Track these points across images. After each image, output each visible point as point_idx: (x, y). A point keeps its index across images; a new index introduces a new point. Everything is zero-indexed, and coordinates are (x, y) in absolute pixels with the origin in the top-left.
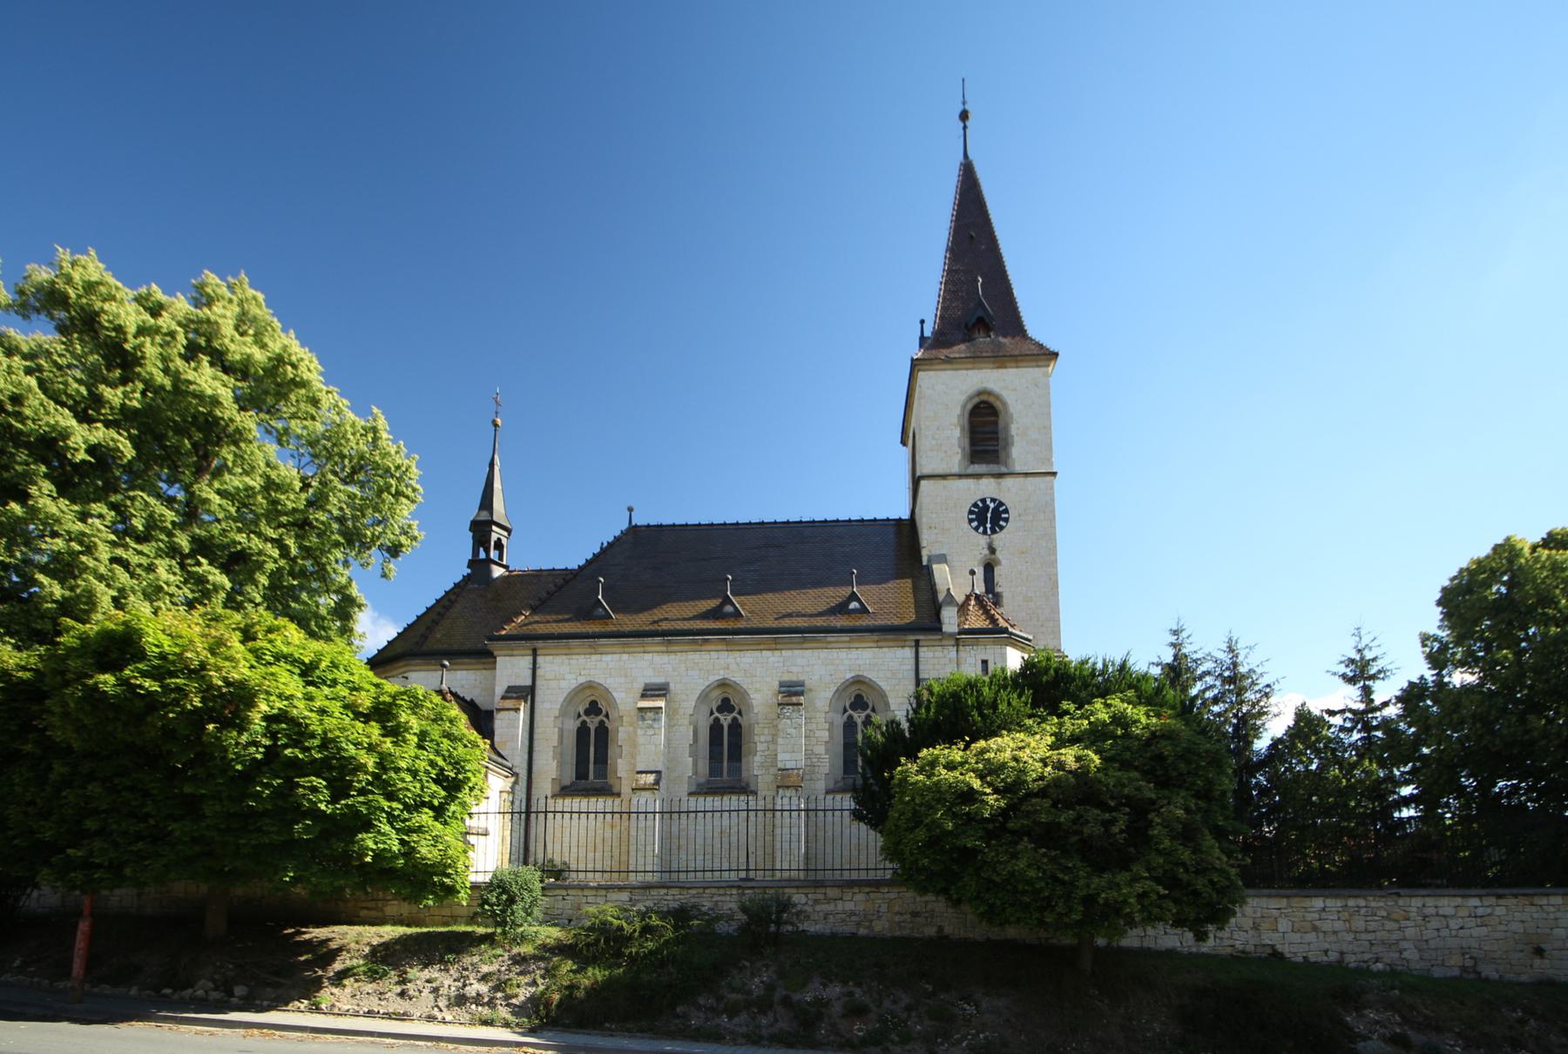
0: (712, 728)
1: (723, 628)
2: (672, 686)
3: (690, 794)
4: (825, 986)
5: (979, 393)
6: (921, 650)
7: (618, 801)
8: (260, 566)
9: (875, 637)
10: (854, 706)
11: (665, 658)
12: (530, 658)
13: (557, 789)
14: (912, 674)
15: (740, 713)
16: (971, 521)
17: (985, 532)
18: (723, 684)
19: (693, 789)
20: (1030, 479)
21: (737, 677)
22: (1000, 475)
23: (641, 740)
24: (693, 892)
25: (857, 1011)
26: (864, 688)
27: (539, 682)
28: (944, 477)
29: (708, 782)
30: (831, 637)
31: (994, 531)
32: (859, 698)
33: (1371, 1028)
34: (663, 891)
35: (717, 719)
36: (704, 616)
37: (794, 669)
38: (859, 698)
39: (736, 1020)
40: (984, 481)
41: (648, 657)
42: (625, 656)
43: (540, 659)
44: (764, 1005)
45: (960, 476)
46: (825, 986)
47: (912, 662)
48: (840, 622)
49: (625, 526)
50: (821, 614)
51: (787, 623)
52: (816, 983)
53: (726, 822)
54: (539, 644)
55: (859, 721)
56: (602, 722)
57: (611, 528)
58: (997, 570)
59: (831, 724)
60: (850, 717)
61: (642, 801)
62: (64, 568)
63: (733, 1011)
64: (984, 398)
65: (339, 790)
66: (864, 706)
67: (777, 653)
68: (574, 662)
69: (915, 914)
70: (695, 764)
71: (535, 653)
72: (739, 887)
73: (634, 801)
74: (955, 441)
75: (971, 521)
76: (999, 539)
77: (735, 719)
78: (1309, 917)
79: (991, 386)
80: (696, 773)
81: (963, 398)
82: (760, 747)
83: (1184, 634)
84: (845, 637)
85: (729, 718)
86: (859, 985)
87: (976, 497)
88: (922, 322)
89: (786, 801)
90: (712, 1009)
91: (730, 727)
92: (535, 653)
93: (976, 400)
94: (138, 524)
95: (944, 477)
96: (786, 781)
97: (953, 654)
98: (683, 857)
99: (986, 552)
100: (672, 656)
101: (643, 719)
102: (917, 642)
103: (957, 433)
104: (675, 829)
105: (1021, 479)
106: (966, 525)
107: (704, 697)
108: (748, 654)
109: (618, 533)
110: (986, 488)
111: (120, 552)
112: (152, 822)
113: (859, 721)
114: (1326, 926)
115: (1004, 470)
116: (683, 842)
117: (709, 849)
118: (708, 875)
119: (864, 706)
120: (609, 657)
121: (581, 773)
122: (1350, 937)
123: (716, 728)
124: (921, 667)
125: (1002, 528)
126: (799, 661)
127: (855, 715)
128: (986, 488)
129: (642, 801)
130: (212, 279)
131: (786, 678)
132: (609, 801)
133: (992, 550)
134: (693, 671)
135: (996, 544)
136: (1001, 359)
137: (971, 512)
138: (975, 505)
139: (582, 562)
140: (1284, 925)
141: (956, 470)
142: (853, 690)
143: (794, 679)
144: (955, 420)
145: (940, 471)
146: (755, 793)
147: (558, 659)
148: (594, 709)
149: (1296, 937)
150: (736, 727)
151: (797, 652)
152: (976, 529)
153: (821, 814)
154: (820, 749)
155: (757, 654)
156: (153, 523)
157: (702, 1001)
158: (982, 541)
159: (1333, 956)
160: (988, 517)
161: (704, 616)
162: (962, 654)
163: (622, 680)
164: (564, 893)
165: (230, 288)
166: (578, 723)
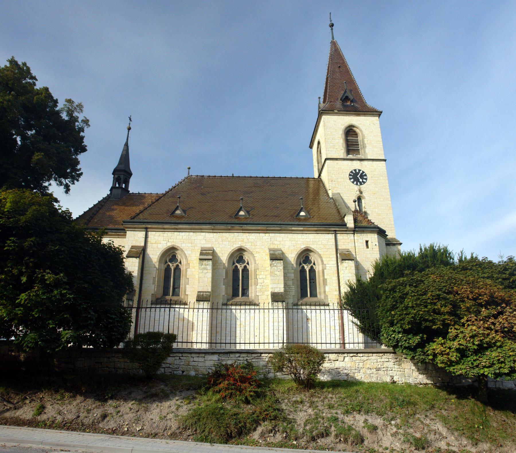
1: (232, 223)
11: (211, 235)
13: (154, 299)
14: (334, 247)
16: (350, 179)
27: (149, 244)
34: (237, 355)
37: (276, 242)
47: (334, 240)
49: (186, 176)
57: (181, 176)
58: (363, 201)
69: (378, 369)
70: (226, 289)
74: (341, 145)
75: (350, 179)
76: (363, 187)
80: (227, 294)
87: (352, 169)
88: (320, 98)
93: (348, 129)
99: (358, 192)
100: (215, 234)
106: (348, 180)
107: (232, 256)
108: (253, 234)
110: (356, 165)
113: (172, 268)
116: (219, 330)
118: (333, 345)
120: (183, 233)
121: (166, 292)
126: (278, 239)
127: (239, 266)
128: (356, 165)
133: (361, 192)
134: (224, 243)
135: (362, 190)
137: (350, 175)
138: (352, 172)
141: (342, 157)
143: (276, 247)
144: (340, 136)
145: (335, 157)
154: (290, 283)
155: (258, 234)
158: (356, 188)
163: (190, 245)
164: (181, 355)
166: (166, 266)
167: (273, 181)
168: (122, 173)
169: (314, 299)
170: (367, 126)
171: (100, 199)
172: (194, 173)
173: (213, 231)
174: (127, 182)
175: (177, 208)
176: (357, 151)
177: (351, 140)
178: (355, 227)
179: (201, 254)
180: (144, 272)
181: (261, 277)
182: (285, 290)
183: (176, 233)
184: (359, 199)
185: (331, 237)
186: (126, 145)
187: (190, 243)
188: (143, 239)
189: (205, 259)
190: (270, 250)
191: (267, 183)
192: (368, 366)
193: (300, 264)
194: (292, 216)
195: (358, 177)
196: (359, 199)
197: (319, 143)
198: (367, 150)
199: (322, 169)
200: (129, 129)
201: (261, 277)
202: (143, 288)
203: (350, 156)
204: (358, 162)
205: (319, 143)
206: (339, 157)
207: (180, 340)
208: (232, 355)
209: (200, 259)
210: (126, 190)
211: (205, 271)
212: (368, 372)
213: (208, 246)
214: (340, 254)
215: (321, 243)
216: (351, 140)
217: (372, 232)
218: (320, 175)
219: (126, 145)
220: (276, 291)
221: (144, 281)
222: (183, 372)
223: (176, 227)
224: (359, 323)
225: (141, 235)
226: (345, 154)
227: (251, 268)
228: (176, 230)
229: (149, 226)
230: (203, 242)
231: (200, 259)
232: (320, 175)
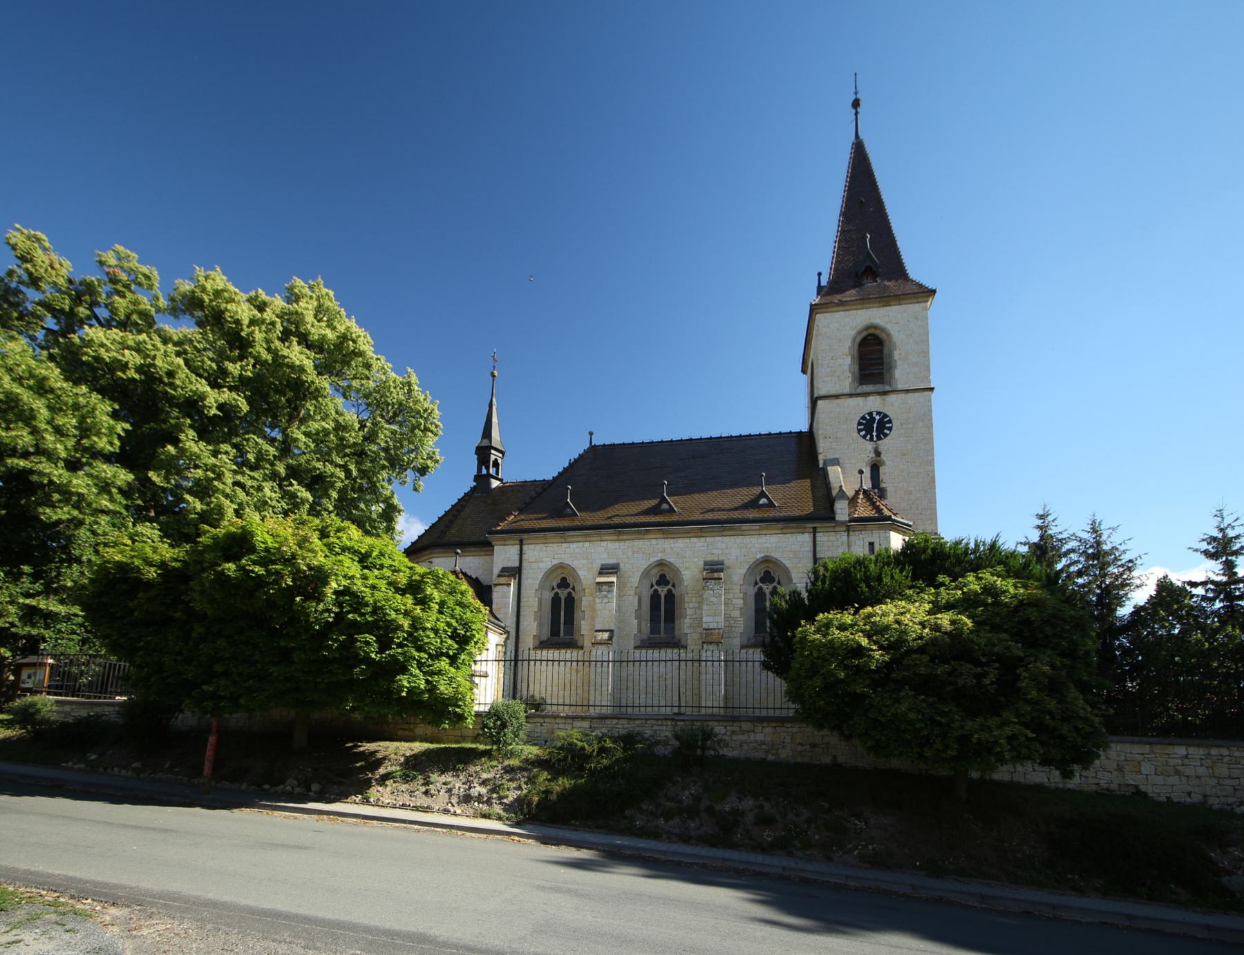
1: (661, 521)
2: (622, 566)
3: (636, 648)
4: (740, 799)
5: (867, 328)
6: (818, 535)
7: (581, 652)
8: (332, 485)
9: (780, 525)
11: (617, 544)
13: (537, 643)
14: (811, 555)
17: (872, 439)
18: (661, 564)
19: (745, 642)
20: (910, 395)
22: (885, 393)
25: (766, 821)
28: (837, 397)
30: (745, 527)
31: (879, 438)
32: (767, 573)
35: (656, 591)
36: (647, 512)
37: (716, 551)
38: (767, 573)
39: (671, 823)
40: (871, 398)
42: (587, 544)
43: (525, 547)
45: (851, 395)
46: (740, 799)
47: (811, 544)
48: (752, 514)
49: (587, 446)
50: (736, 509)
51: (710, 516)
54: (525, 536)
55: (767, 592)
56: (570, 593)
57: (577, 448)
58: (882, 470)
59: (745, 594)
61: (599, 653)
62: (203, 490)
65: (384, 645)
69: (814, 745)
70: (639, 625)
71: (521, 543)
72: (673, 720)
73: (593, 653)
74: (846, 368)
75: (859, 431)
76: (884, 444)
78: (1172, 762)
79: (878, 321)
80: (640, 631)
81: (854, 333)
83: (1050, 518)
84: (756, 526)
85: (665, 590)
88: (820, 274)
91: (666, 596)
92: (521, 543)
93: (864, 334)
94: (251, 457)
95: (837, 397)
96: (710, 638)
97: (845, 538)
99: (872, 455)
100: (622, 543)
102: (815, 529)
103: (848, 361)
105: (903, 396)
106: (856, 434)
107: (646, 573)
108: (680, 540)
109: (581, 452)
110: (873, 404)
111: (239, 477)
112: (259, 666)
113: (767, 592)
114: (1189, 771)
115: (888, 388)
116: (630, 684)
122: (1213, 782)
123: (655, 597)
124: (818, 549)
125: (886, 435)
128: (873, 404)
130: (299, 282)
131: (709, 558)
132: (575, 652)
133: (878, 453)
134: (637, 554)
135: (881, 449)
137: (859, 424)
138: (863, 418)
139: (556, 474)
140: (1147, 768)
141: (847, 391)
144: (846, 351)
145: (833, 392)
148: (564, 583)
149: (1159, 780)
150: (670, 597)
154: (736, 614)
155: (687, 540)
156: (260, 456)
157: (644, 807)
158: (869, 446)
159: (1196, 798)
160: (875, 427)
161: (647, 512)
162: (852, 538)
163: (584, 562)
165: (311, 288)
166: (552, 594)
171: (461, 495)
172: (598, 441)
180: (522, 604)
183: (564, 545)
185: (807, 538)
188: (517, 557)
192: (798, 740)
198: (898, 373)
202: (521, 628)
203: (866, 388)
204: (878, 397)
206: (840, 392)
207: (757, 664)
211: (606, 600)
212: (799, 748)
221: (522, 618)
225: (513, 550)
227: (676, 592)
230: (605, 556)
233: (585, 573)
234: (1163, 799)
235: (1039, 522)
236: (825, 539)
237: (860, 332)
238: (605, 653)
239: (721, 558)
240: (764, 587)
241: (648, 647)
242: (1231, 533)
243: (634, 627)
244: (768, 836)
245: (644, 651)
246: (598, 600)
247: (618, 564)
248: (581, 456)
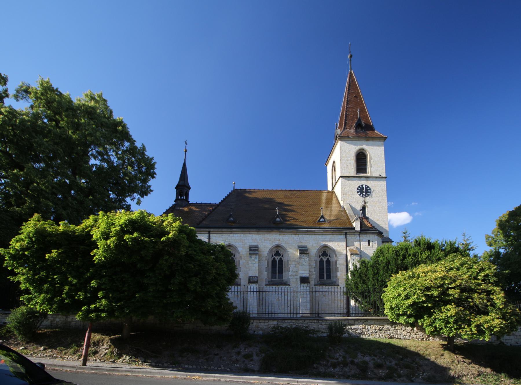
0: (320, 261)
2: (259, 246)
3: (266, 285)
4: (364, 357)
6: (347, 236)
7: (239, 287)
10: (276, 255)
11: (257, 236)
12: (208, 235)
15: (282, 256)
16: (358, 192)
17: (363, 196)
18: (278, 246)
19: (267, 283)
21: (283, 244)
23: (250, 265)
24: (300, 321)
25: (379, 366)
26: (327, 249)
29: (272, 281)
31: (366, 196)
32: (325, 252)
33: (255, 365)
34: (289, 321)
35: (274, 258)
37: (303, 241)
38: (325, 252)
39: (336, 370)
41: (251, 235)
42: (242, 235)
43: (211, 235)
44: (345, 364)
46: (364, 357)
49: (232, 189)
52: (360, 355)
53: (280, 296)
55: (325, 261)
56: (281, 258)
59: (316, 261)
60: (322, 259)
61: (252, 287)
63: (334, 366)
64: (362, 151)
66: (327, 255)
67: (297, 235)
68: (223, 236)
70: (268, 274)
71: (209, 234)
72: (318, 320)
73: (249, 287)
75: (358, 192)
76: (367, 199)
77: (281, 258)
80: (268, 277)
82: (291, 269)
83: (408, 233)
85: (279, 258)
86: (376, 356)
89: (302, 288)
90: (326, 365)
91: (279, 261)
92: (209, 234)
96: (252, 280)
97: (358, 238)
98: (264, 308)
99: (363, 203)
100: (259, 236)
101: (251, 258)
102: (346, 233)
104: (261, 297)
106: (356, 193)
107: (271, 250)
108: (287, 235)
109: (230, 192)
110: (364, 183)
112: (126, 293)
113: (325, 261)
116: (264, 302)
117: (273, 305)
119: (327, 255)
120: (237, 235)
123: (274, 261)
128: (364, 183)
129: (252, 287)
131: (300, 244)
132: (236, 287)
133: (365, 203)
134: (266, 241)
135: (366, 201)
136: (368, 139)
137: (358, 189)
138: (359, 187)
139: (220, 201)
142: (323, 250)
143: (303, 245)
144: (352, 158)
146: (289, 285)
147: (218, 235)
148: (277, 254)
150: (281, 261)
151: (304, 235)
152: (360, 195)
153: (336, 293)
154: (313, 270)
155: (290, 235)
157: (322, 363)
158: (362, 199)
162: (361, 238)
163: (241, 243)
167: (298, 194)
168: (183, 188)
169: (329, 281)
170: (376, 154)
172: (236, 188)
173: (258, 233)
174: (187, 195)
175: (231, 216)
176: (365, 171)
177: (361, 161)
178: (361, 230)
179: (250, 250)
181: (292, 266)
182: (309, 275)
183: (231, 235)
184: (364, 208)
186: (184, 165)
187: (239, 241)
189: (254, 254)
190: (299, 247)
191: (294, 195)
193: (320, 257)
194: (314, 221)
195: (364, 191)
196: (364, 208)
197: (334, 162)
199: (336, 183)
200: (186, 151)
201: (292, 266)
205: (334, 162)
206: (350, 175)
208: (286, 321)
209: (250, 254)
210: (187, 200)
211: (254, 262)
213: (255, 244)
214: (349, 250)
215: (338, 245)
216: (361, 161)
217: (373, 234)
218: (333, 188)
219: (184, 165)
220: (304, 275)
222: (254, 332)
223: (231, 230)
224: (247, 195)
226: (355, 172)
227: (284, 259)
228: (232, 232)
229: (212, 230)
231: (250, 254)
232: (333, 188)
233: (241, 249)
234: (509, 345)
235: (404, 235)
236: (350, 238)
237: (357, 151)
238: (255, 287)
239: (305, 245)
240: (276, 258)
241: (272, 285)
242: (468, 242)
243: (265, 275)
244: (382, 373)
245: (271, 287)
246: (250, 262)
247: (258, 245)
248: (230, 193)
